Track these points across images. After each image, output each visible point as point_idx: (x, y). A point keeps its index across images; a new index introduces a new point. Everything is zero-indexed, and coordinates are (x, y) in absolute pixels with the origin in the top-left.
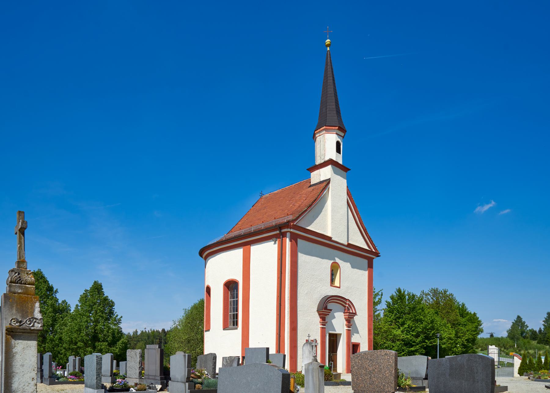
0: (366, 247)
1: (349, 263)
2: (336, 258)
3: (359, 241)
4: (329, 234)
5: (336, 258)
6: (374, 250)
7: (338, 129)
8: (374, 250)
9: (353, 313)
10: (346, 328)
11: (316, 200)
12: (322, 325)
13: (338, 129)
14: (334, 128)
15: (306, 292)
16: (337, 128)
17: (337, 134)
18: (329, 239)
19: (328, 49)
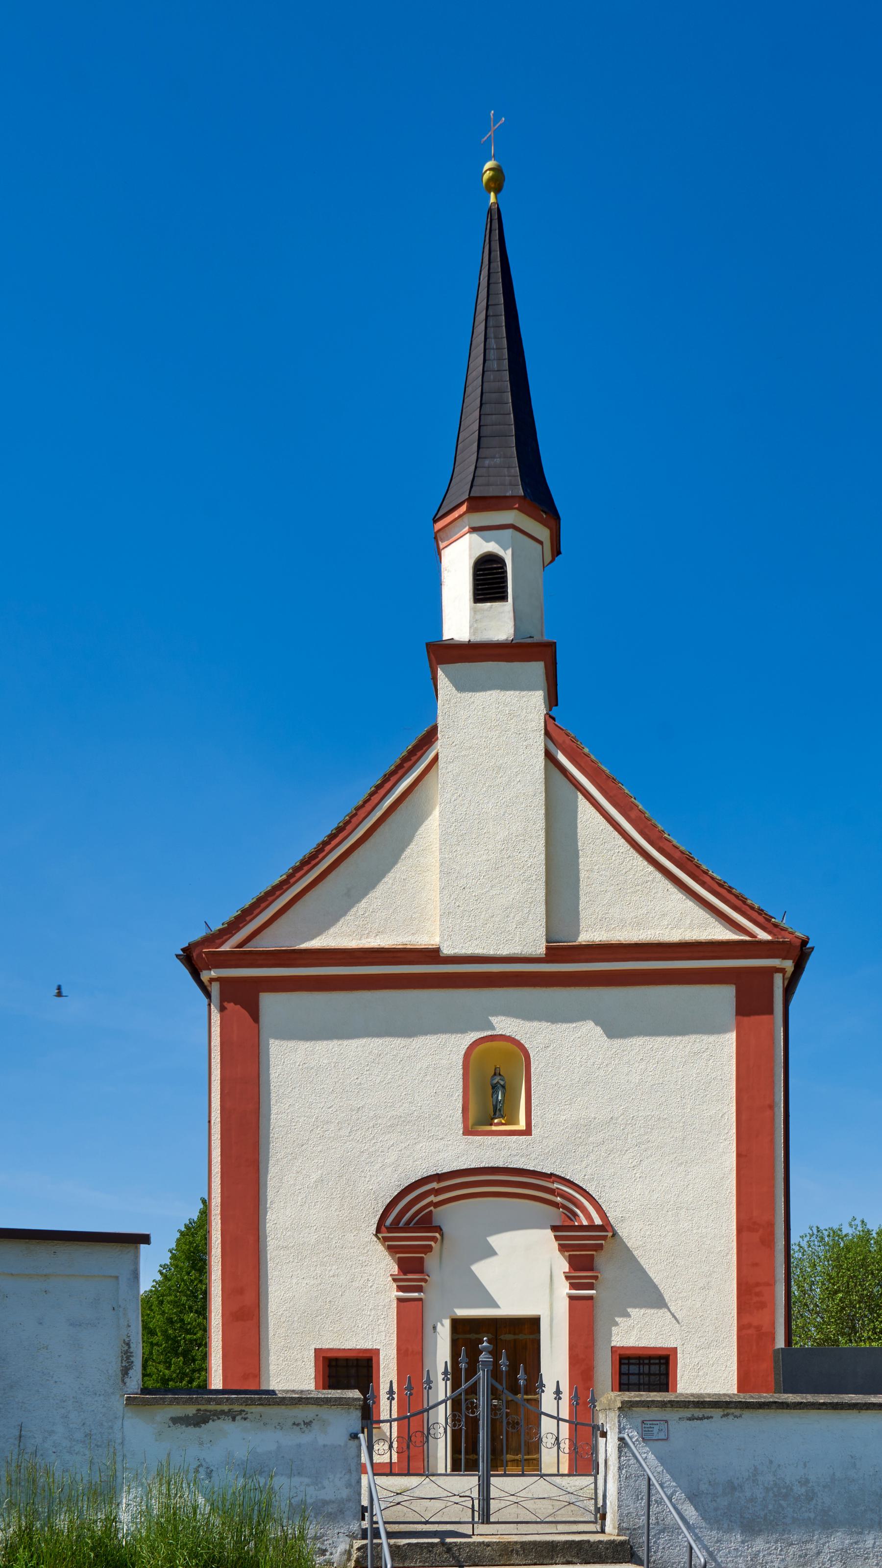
0: (722, 933)
1: (590, 1024)
2: (494, 1020)
3: (674, 917)
4: (426, 937)
5: (494, 1020)
6: (763, 936)
7: (470, 510)
8: (763, 936)
9: (592, 1227)
10: (564, 1289)
11: (347, 823)
12: (400, 1289)
13: (470, 510)
14: (456, 514)
15: (314, 1177)
16: (464, 508)
17: (474, 530)
18: (432, 955)
19: (492, 198)
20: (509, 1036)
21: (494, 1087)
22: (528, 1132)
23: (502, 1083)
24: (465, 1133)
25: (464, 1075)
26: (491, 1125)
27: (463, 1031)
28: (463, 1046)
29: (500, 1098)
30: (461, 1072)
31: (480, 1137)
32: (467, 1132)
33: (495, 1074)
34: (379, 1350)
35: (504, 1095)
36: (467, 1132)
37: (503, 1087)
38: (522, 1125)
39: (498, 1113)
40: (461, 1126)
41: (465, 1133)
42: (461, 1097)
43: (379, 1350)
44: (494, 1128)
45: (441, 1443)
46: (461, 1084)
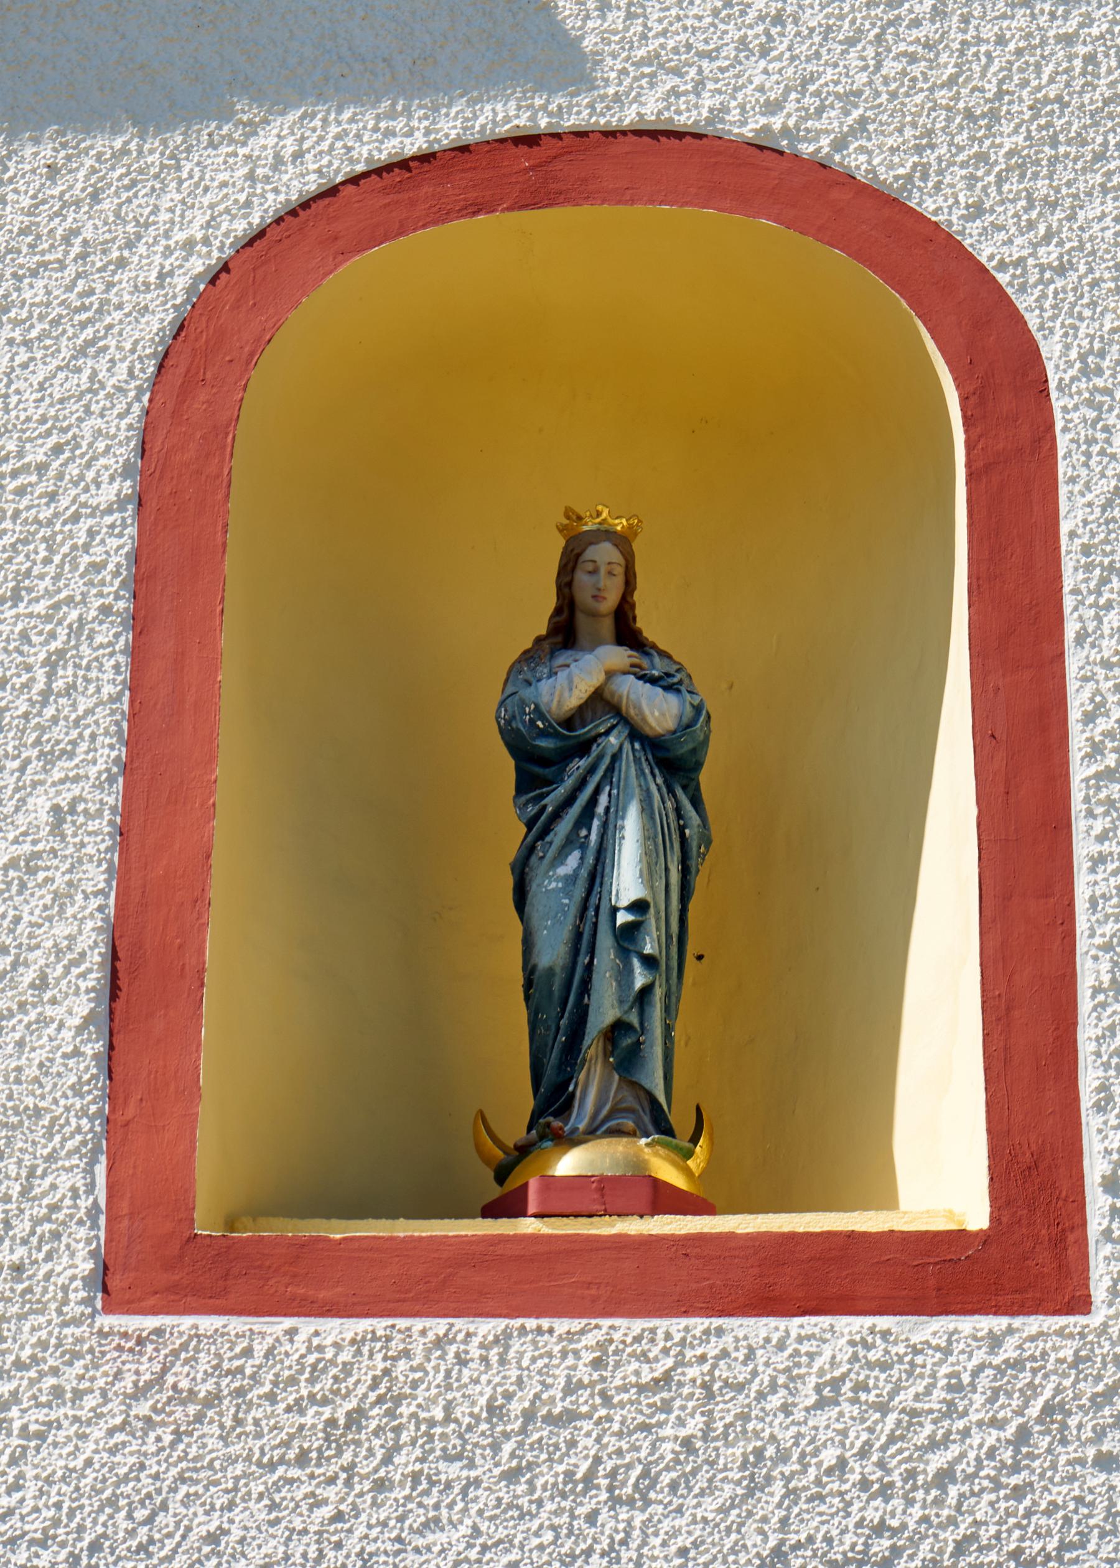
20: (760, 149)
21: (549, 760)
22: (1018, 1259)
23: (659, 711)
24: (120, 1282)
25: (145, 574)
26: (511, 1206)
27: (171, 96)
28: (147, 261)
29: (627, 882)
30: (117, 545)
31: (335, 1329)
32: (164, 1258)
33: (565, 633)
34: (1080, 1304)
35: (682, 855)
36: (164, 1258)
37: (675, 762)
38: (938, 1170)
39: (593, 1086)
40: (76, 1185)
41: (120, 1282)
42: (96, 837)
43: (1080, 1304)
44: (578, 1094)
45: (658, 1005)
46: (110, 677)
